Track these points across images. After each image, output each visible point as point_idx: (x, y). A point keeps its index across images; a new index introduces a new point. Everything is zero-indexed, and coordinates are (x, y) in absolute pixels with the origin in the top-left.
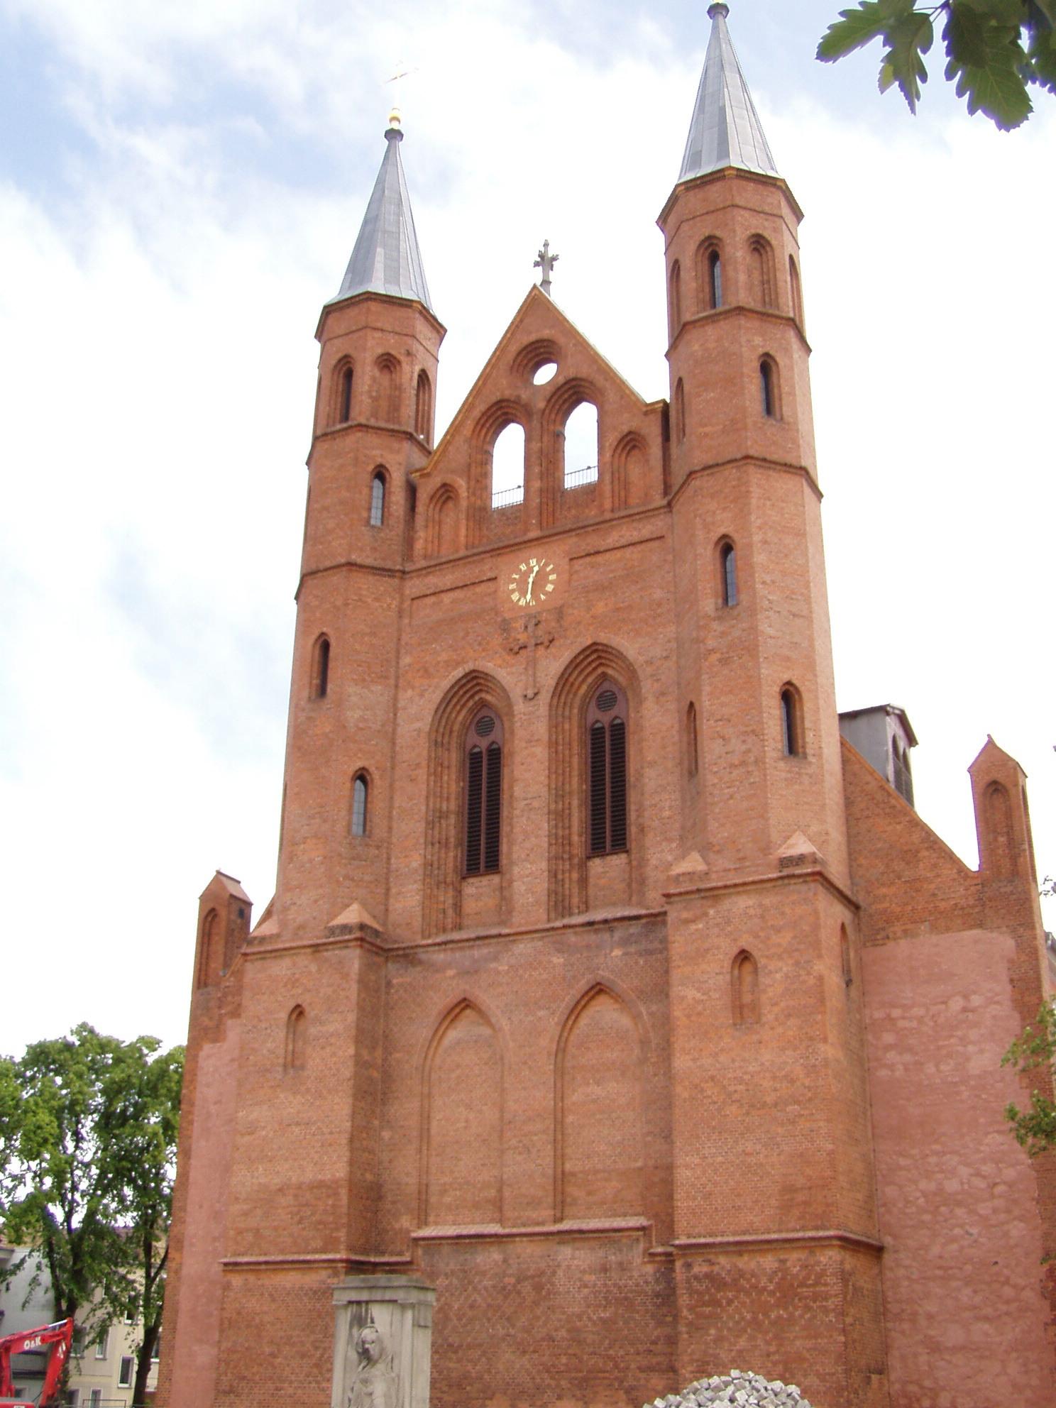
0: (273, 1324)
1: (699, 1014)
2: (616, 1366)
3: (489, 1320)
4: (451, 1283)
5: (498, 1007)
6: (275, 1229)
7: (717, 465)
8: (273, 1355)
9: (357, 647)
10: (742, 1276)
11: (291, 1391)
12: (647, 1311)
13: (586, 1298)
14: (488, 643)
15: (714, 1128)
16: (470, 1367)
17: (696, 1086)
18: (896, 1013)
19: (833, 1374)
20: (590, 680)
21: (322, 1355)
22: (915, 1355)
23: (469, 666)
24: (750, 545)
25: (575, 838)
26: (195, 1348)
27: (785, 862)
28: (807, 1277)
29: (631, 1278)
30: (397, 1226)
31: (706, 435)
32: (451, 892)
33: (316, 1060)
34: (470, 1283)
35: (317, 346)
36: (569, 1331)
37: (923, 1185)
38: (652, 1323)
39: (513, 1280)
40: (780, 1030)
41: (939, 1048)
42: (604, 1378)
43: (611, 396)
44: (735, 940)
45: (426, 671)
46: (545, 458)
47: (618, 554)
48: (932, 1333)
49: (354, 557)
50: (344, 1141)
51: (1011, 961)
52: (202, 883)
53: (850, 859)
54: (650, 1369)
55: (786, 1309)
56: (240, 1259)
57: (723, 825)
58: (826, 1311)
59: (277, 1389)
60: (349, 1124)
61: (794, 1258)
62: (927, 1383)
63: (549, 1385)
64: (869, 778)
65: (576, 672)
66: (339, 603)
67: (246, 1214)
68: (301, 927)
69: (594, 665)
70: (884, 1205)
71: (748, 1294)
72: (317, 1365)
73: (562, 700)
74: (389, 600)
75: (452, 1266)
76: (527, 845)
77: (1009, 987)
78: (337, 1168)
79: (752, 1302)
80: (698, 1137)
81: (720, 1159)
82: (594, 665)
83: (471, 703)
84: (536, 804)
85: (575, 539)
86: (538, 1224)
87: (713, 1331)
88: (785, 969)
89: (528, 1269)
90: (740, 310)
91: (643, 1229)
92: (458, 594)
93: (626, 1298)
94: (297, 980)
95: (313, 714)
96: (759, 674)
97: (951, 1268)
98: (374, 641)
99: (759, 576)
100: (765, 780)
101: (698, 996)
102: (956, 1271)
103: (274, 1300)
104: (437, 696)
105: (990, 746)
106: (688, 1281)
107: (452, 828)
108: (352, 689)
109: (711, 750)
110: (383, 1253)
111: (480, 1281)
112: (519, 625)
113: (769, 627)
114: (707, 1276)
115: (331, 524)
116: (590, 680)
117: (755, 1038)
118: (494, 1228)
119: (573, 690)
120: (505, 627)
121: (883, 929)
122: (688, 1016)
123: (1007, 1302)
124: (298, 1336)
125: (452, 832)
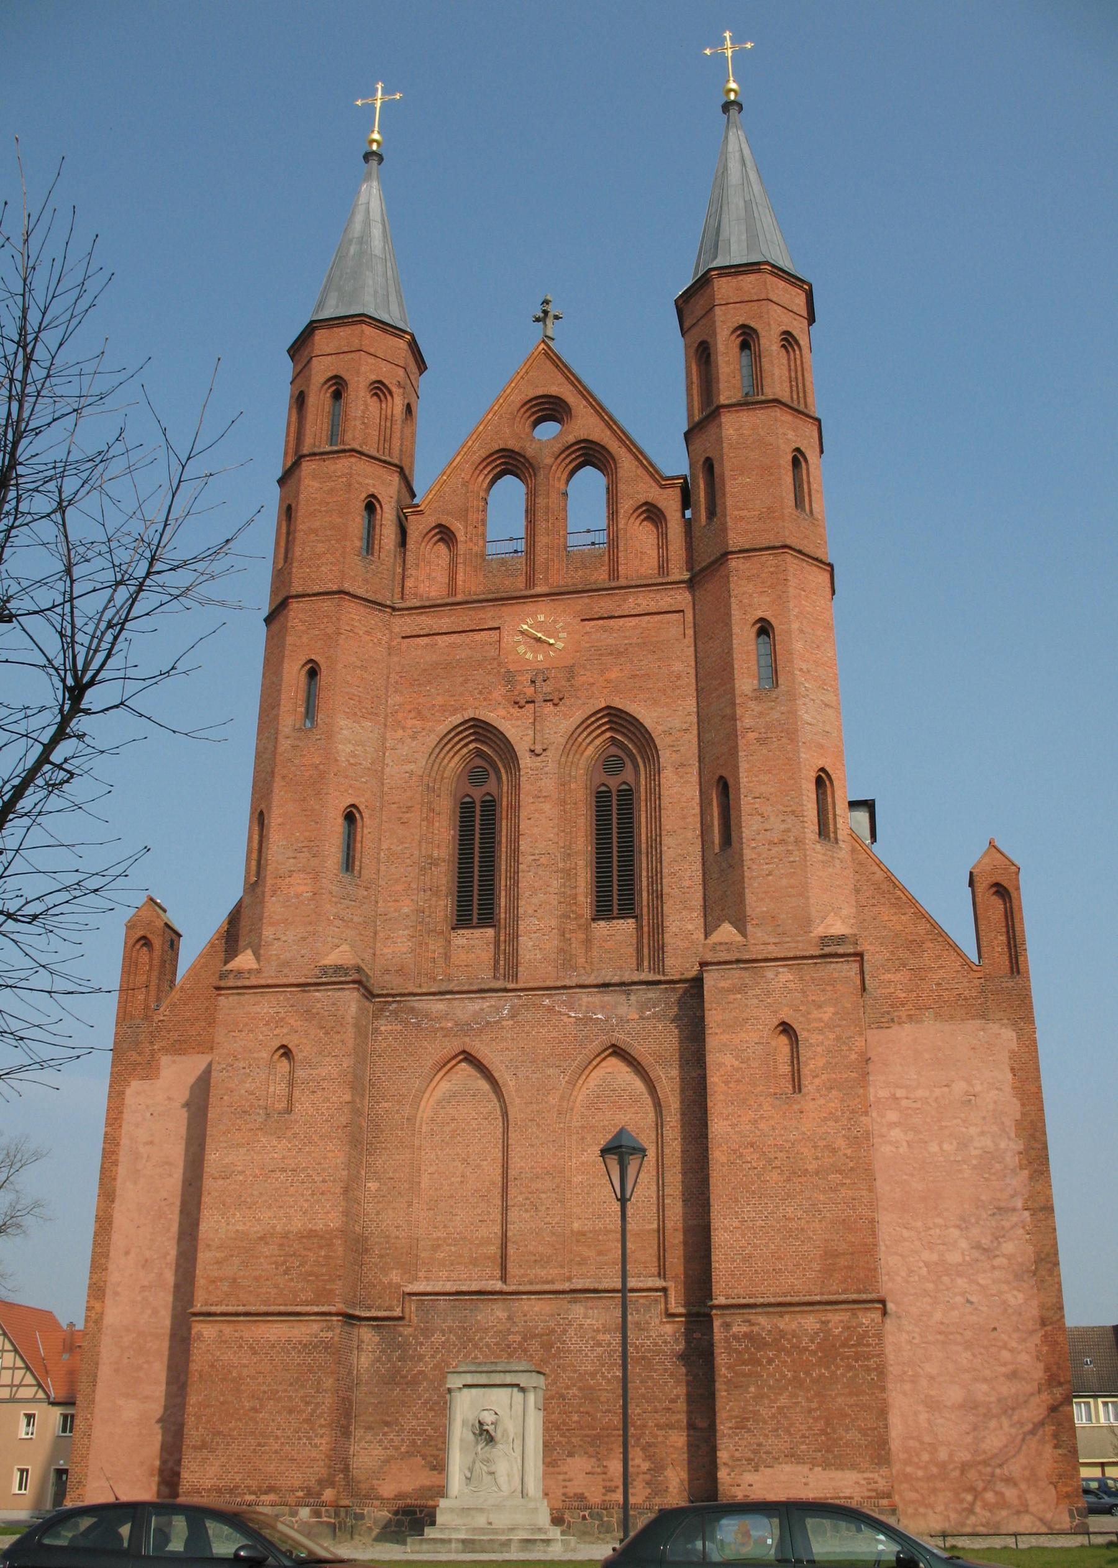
0: (253, 1378)
1: (738, 1081)
5: (502, 1062)
6: (257, 1279)
7: (755, 550)
8: (255, 1410)
9: (349, 678)
10: (782, 1337)
11: (276, 1447)
12: (666, 1370)
13: (599, 1357)
14: (490, 693)
15: (754, 1192)
17: (735, 1151)
18: (900, 1093)
19: (875, 1429)
21: (314, 1411)
22: (916, 1413)
23: (470, 714)
24: (789, 632)
25: (581, 899)
26: (120, 1402)
27: (825, 940)
28: (850, 1338)
30: (385, 1281)
31: (742, 518)
32: (441, 942)
33: (304, 1105)
34: (470, 1340)
36: (580, 1389)
37: (926, 1255)
39: (518, 1338)
40: (822, 1101)
41: (941, 1128)
45: (419, 713)
47: (634, 621)
48: (933, 1393)
49: (347, 586)
50: (338, 1190)
51: (1012, 1052)
55: (827, 1368)
56: (213, 1309)
57: (762, 899)
58: (868, 1370)
59: (259, 1445)
60: (345, 1173)
61: (837, 1319)
62: (927, 1439)
63: (559, 1442)
64: (876, 868)
65: (585, 733)
66: (330, 631)
68: (286, 963)
69: (604, 728)
70: (888, 1274)
71: (789, 1353)
72: (307, 1421)
73: (570, 760)
74: (379, 635)
75: (449, 1323)
76: (535, 900)
77: (1010, 1076)
79: (793, 1361)
80: (737, 1201)
81: (760, 1223)
82: (604, 728)
85: (587, 601)
86: (548, 1283)
87: (752, 1389)
88: (826, 1043)
89: (536, 1327)
90: (777, 401)
91: (664, 1290)
94: (282, 1019)
95: (297, 743)
96: (799, 758)
97: (952, 1333)
98: (365, 675)
99: (799, 664)
100: (805, 861)
102: (958, 1336)
103: (255, 1353)
104: (433, 739)
106: (727, 1340)
107: (444, 876)
108: (342, 722)
109: (750, 827)
110: (369, 1308)
111: (481, 1339)
113: (808, 713)
114: (745, 1335)
115: (320, 548)
117: (796, 1107)
118: (499, 1286)
119: (580, 751)
121: (888, 1013)
122: (726, 1083)
123: (1005, 1364)
124: (286, 1391)
125: (444, 881)
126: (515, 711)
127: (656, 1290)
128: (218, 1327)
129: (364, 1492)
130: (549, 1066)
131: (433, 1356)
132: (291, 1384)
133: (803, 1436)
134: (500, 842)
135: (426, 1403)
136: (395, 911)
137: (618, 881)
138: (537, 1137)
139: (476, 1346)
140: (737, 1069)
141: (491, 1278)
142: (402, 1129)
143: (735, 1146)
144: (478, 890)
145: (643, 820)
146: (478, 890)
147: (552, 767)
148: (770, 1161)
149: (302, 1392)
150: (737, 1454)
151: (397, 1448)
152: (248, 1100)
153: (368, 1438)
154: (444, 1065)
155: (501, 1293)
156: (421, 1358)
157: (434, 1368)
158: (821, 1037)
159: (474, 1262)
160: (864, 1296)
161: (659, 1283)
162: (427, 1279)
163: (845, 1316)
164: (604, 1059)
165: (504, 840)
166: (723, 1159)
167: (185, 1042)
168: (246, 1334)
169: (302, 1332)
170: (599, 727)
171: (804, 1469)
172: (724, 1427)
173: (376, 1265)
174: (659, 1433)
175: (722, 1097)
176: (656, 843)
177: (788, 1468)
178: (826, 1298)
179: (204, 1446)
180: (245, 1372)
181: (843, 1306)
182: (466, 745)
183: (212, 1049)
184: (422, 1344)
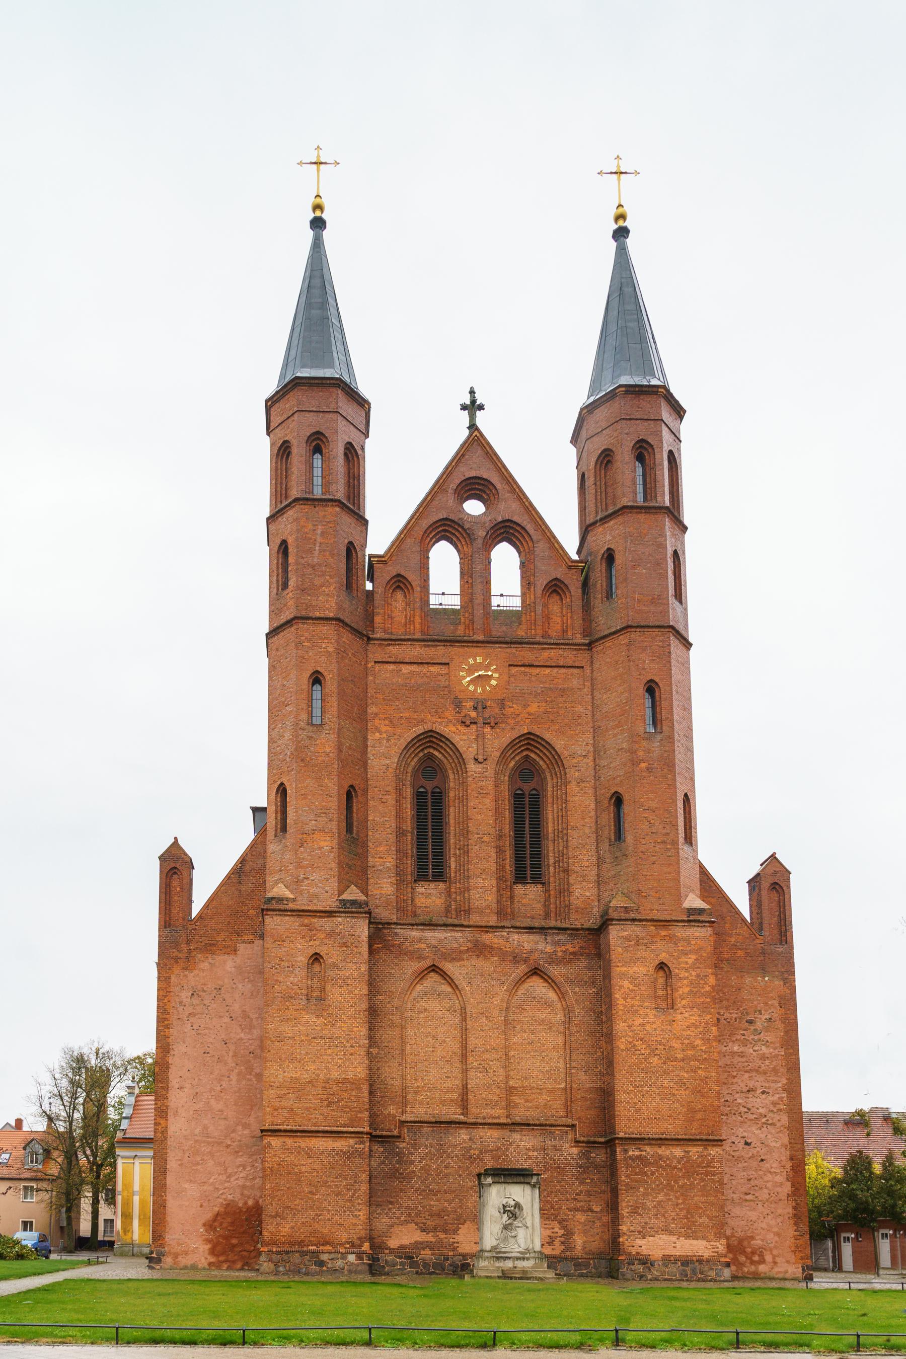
2: (552, 1207)
3: (460, 1176)
4: (430, 1152)
5: (460, 974)
7: (649, 627)
11: (329, 1216)
15: (642, 1069)
17: (630, 1043)
20: (517, 758)
21: (354, 1195)
23: (428, 727)
33: (335, 995)
35: (573, 451)
38: (577, 1183)
39: (477, 1152)
43: (541, 548)
44: (657, 955)
45: (391, 722)
46: (475, 577)
52: (164, 846)
54: (576, 1209)
55: (689, 1179)
58: (714, 1181)
61: (695, 1151)
67: (280, 1097)
78: (360, 1072)
79: (667, 1174)
83: (421, 754)
84: (486, 838)
86: (495, 1118)
87: (641, 1190)
91: (573, 1126)
92: (414, 668)
93: (559, 1167)
101: (631, 987)
103: (310, 1157)
104: (403, 743)
105: (773, 856)
106: (625, 1159)
110: (382, 1130)
111: (452, 1152)
112: (469, 704)
114: (637, 1157)
116: (517, 758)
120: (458, 704)
122: (625, 999)
126: (462, 728)
127: (567, 1126)
128: (281, 1139)
130: (492, 979)
131: (420, 1162)
132: (337, 1177)
133: (673, 1219)
134: (448, 824)
135: (417, 1190)
136: (381, 865)
137: (528, 858)
139: (448, 1156)
140: (632, 991)
141: (455, 1114)
143: (630, 1040)
144: (429, 853)
145: (550, 817)
146: (429, 853)
147: (490, 773)
148: (653, 1051)
149: (345, 1182)
150: (632, 1228)
151: (398, 1218)
152: (293, 990)
154: (421, 975)
155: (465, 1123)
156: (412, 1162)
157: (422, 1168)
158: (687, 974)
160: (711, 1137)
161: (570, 1122)
163: (700, 1149)
165: (452, 821)
166: (623, 1047)
167: (214, 945)
168: (303, 1145)
169: (340, 1144)
170: (520, 747)
171: (674, 1238)
172: (624, 1211)
175: (622, 1008)
176: (562, 834)
177: (664, 1237)
178: (687, 1137)
179: (277, 1215)
180: (303, 1169)
181: (699, 1143)
182: (422, 750)
183: (235, 951)
184: (412, 1154)
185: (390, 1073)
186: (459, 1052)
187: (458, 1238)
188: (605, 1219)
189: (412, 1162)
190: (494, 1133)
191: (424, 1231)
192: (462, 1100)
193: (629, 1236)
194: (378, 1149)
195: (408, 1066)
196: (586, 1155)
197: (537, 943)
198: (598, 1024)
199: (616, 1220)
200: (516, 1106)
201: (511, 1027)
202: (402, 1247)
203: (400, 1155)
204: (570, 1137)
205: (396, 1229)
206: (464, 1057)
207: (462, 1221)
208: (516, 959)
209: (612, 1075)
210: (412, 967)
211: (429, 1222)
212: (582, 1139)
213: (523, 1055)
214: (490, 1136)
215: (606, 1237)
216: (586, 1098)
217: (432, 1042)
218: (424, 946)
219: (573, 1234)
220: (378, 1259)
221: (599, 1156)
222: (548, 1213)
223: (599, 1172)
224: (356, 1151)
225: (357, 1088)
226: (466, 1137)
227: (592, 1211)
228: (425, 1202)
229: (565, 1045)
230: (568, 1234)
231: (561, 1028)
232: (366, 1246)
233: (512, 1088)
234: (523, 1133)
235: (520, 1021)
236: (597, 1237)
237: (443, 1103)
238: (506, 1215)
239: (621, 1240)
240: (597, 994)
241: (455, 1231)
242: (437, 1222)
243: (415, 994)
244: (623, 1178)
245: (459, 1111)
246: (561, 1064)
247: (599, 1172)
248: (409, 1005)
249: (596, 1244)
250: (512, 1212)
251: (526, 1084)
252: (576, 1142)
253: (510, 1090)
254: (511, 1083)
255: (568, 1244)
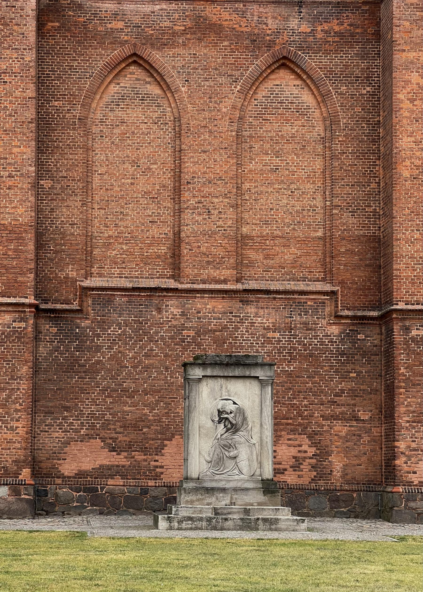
2: (300, 415)
3: (167, 369)
16: (146, 411)
21: (9, 397)
29: (316, 337)
34: (145, 333)
38: (337, 379)
39: (192, 333)
42: (288, 424)
53: (38, 30)
89: (209, 323)
91: (333, 293)
106: (406, 342)
110: (56, 301)
111: (157, 333)
118: (172, 284)
122: (412, 101)
129: (45, 471)
130: (220, 74)
131: (110, 348)
135: (104, 390)
138: (210, 144)
142: (74, 129)
150: (414, 445)
151: (77, 431)
153: (48, 422)
154: (116, 69)
155: (176, 290)
156: (98, 348)
159: (146, 261)
161: (328, 288)
162: (100, 275)
164: (273, 72)
172: (403, 419)
173: (52, 260)
174: (324, 423)
175: (407, 114)
184: (98, 336)
185: (68, 213)
186: (170, 183)
187: (162, 460)
188: (375, 432)
189: (98, 348)
190: (219, 305)
191: (113, 450)
192: (173, 256)
193: (409, 457)
194: (49, 328)
195: (96, 206)
196: (349, 336)
197: (286, 19)
198: (374, 141)
199: (391, 435)
200: (251, 264)
201: (246, 146)
202: (81, 474)
203: (81, 337)
204: (328, 310)
205: (73, 448)
206: (177, 192)
207: (169, 435)
208: (256, 42)
209: (389, 216)
210: (103, 57)
211: (121, 437)
212: (346, 313)
213: (264, 189)
214: (212, 309)
215: (377, 458)
216: (352, 252)
217: (131, 170)
218: (120, 25)
219: (329, 454)
220: (46, 493)
221: (370, 338)
222: (282, 425)
223: (369, 362)
224: (15, 332)
225: (18, 239)
226: (177, 311)
227: (357, 420)
228: (117, 408)
229: (324, 172)
230: (323, 454)
231: (320, 148)
232: (25, 474)
233: (245, 237)
234: (260, 304)
235: (261, 138)
236: (364, 459)
237: (146, 261)
238: (222, 425)
239: (397, 462)
240: (373, 95)
241: (159, 450)
242: (132, 436)
243: (107, 98)
244: (402, 370)
245: (168, 272)
246: (319, 202)
247: (369, 362)
248: (99, 116)
249: (363, 469)
250: (230, 422)
251: (266, 231)
252: (337, 317)
253: (241, 241)
254: (245, 230)
255: (321, 472)
